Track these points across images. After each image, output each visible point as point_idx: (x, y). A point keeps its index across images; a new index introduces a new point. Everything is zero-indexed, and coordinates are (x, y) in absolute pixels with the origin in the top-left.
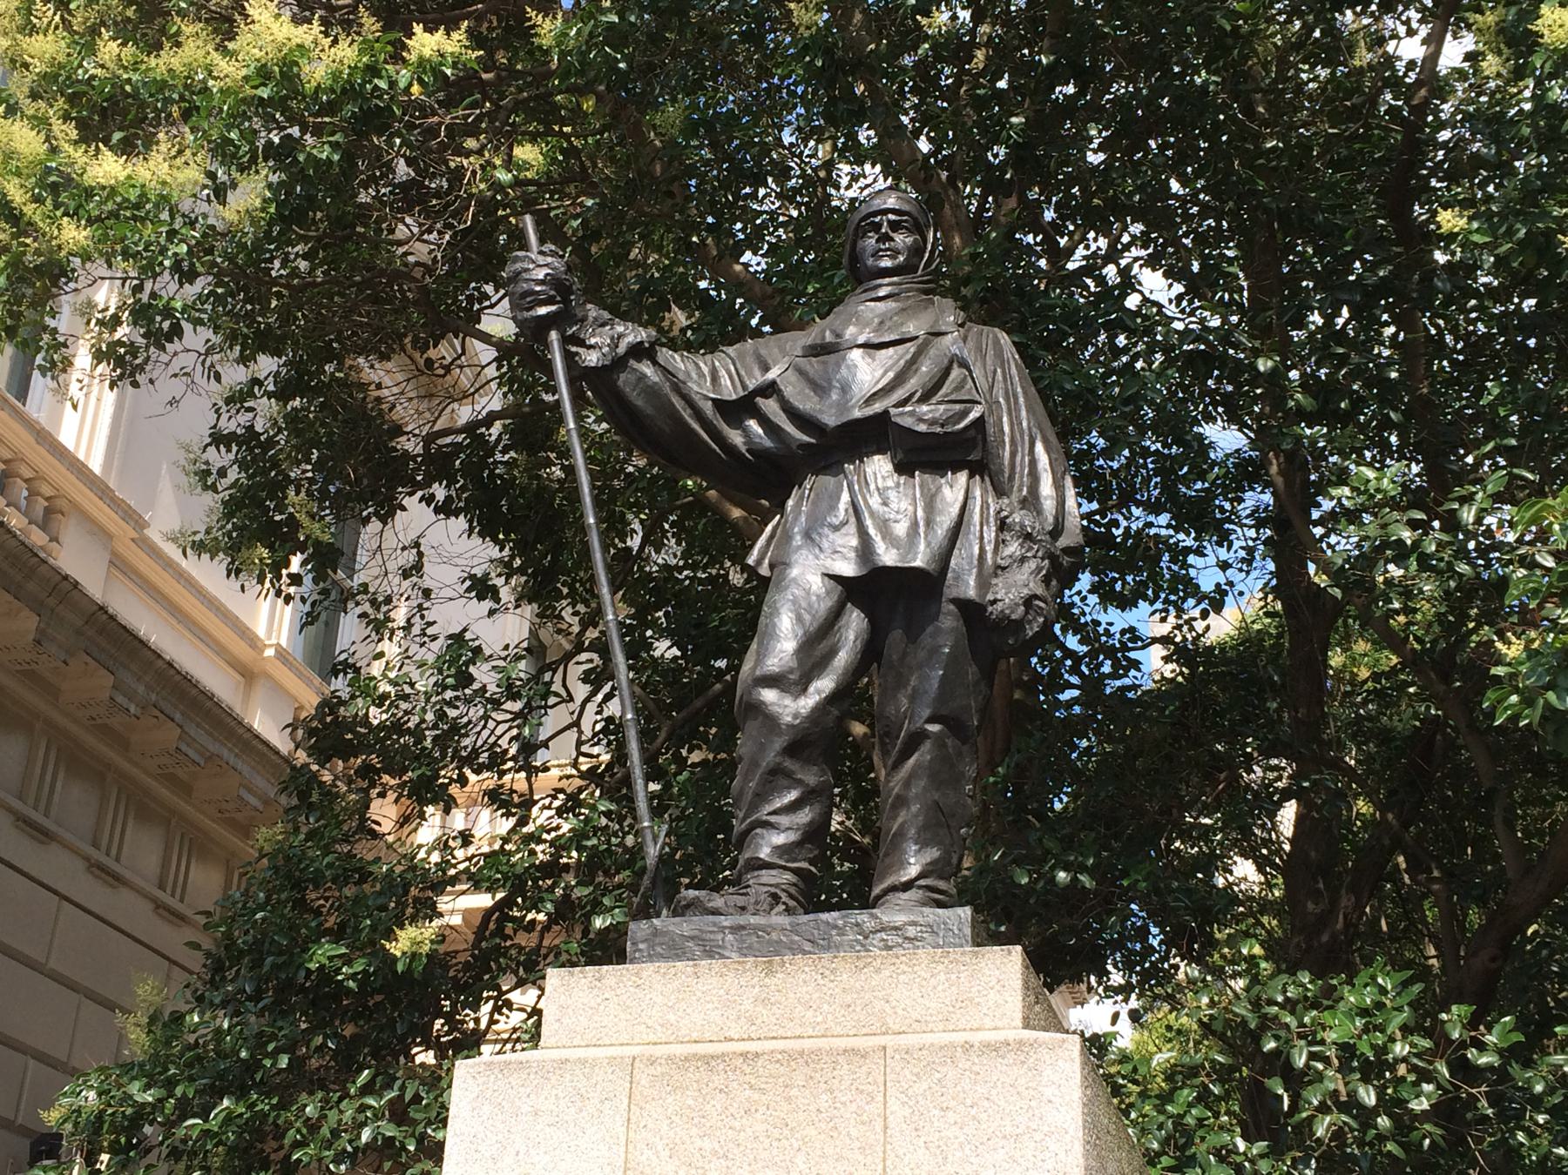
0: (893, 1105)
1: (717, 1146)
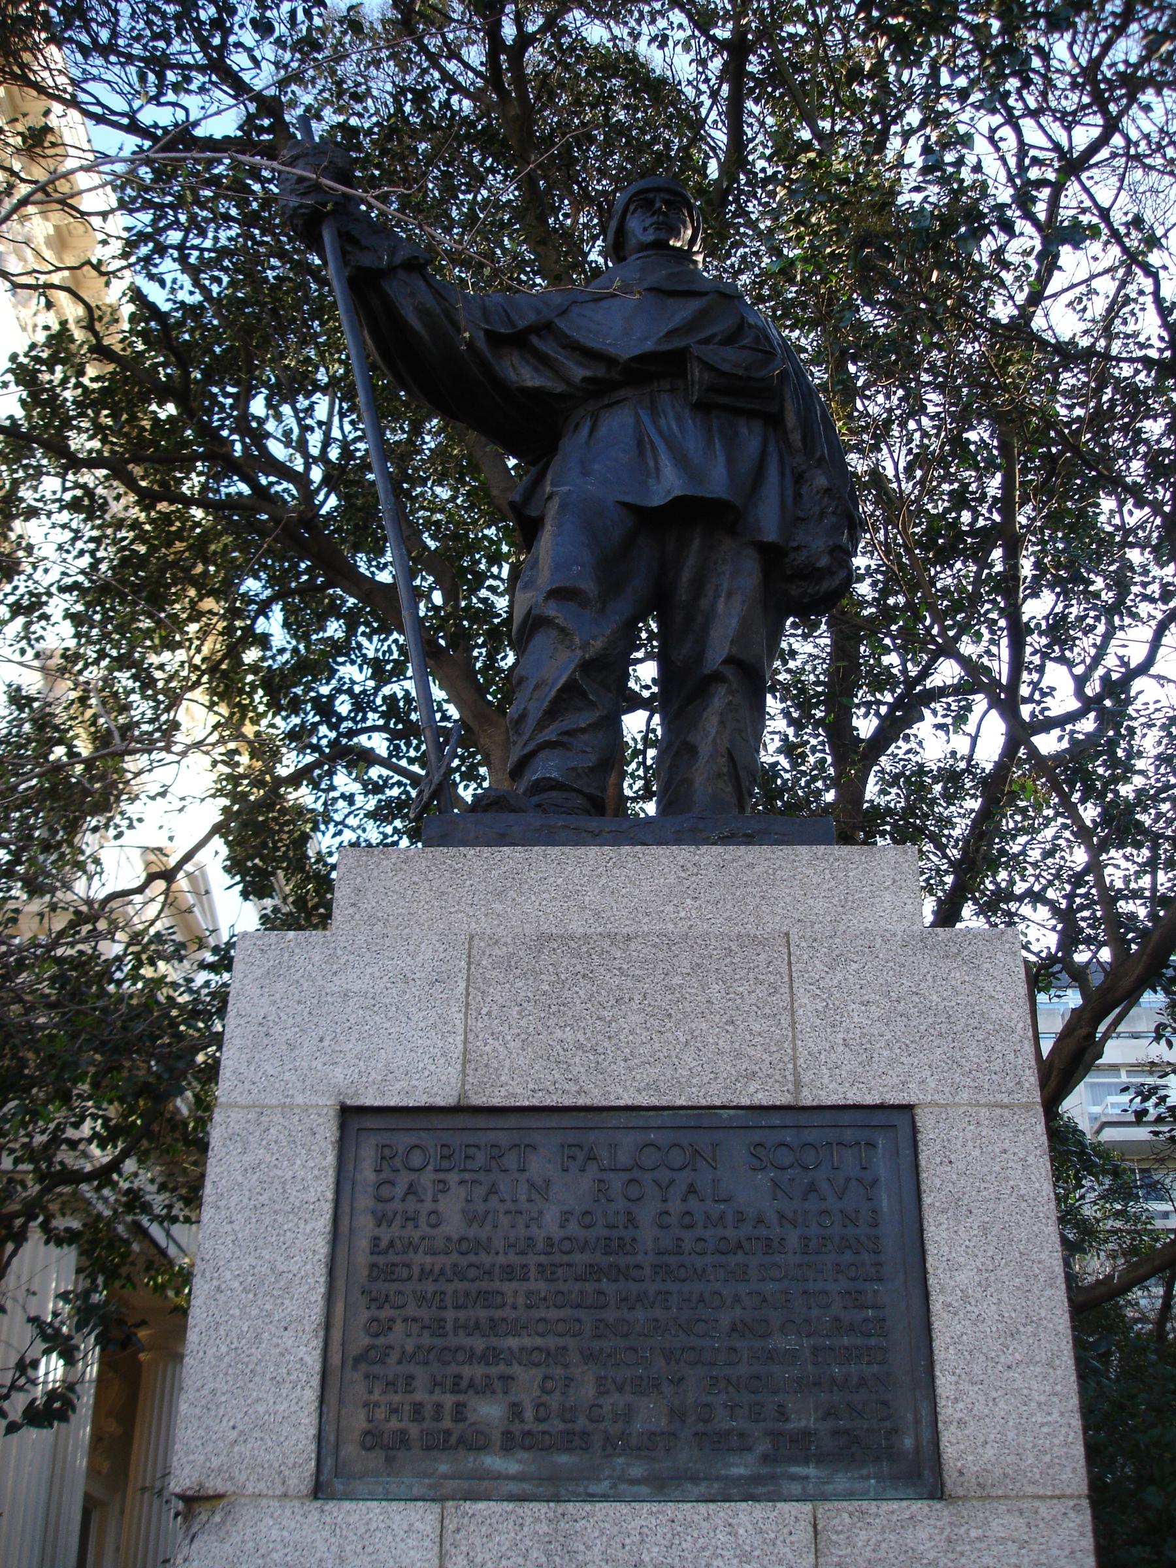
0: (803, 998)
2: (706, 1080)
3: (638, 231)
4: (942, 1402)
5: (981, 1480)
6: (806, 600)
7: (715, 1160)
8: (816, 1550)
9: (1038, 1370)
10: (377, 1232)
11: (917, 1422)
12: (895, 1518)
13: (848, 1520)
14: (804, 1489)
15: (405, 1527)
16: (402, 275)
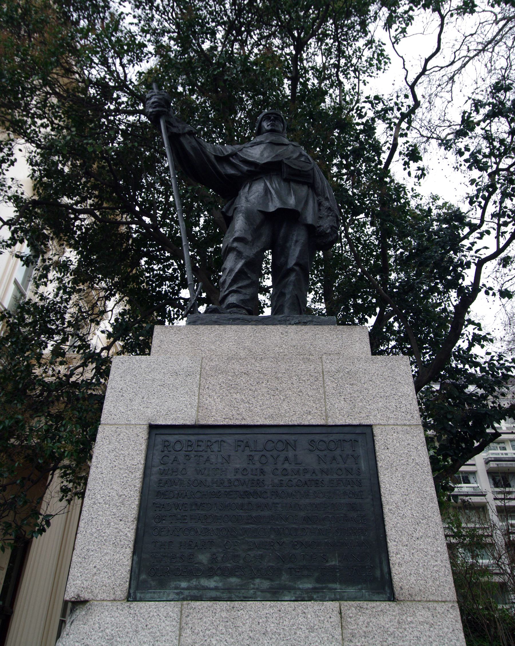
3: (266, 127)
4: (391, 554)
7: (295, 446)
8: (342, 626)
13: (354, 611)
15: (165, 615)
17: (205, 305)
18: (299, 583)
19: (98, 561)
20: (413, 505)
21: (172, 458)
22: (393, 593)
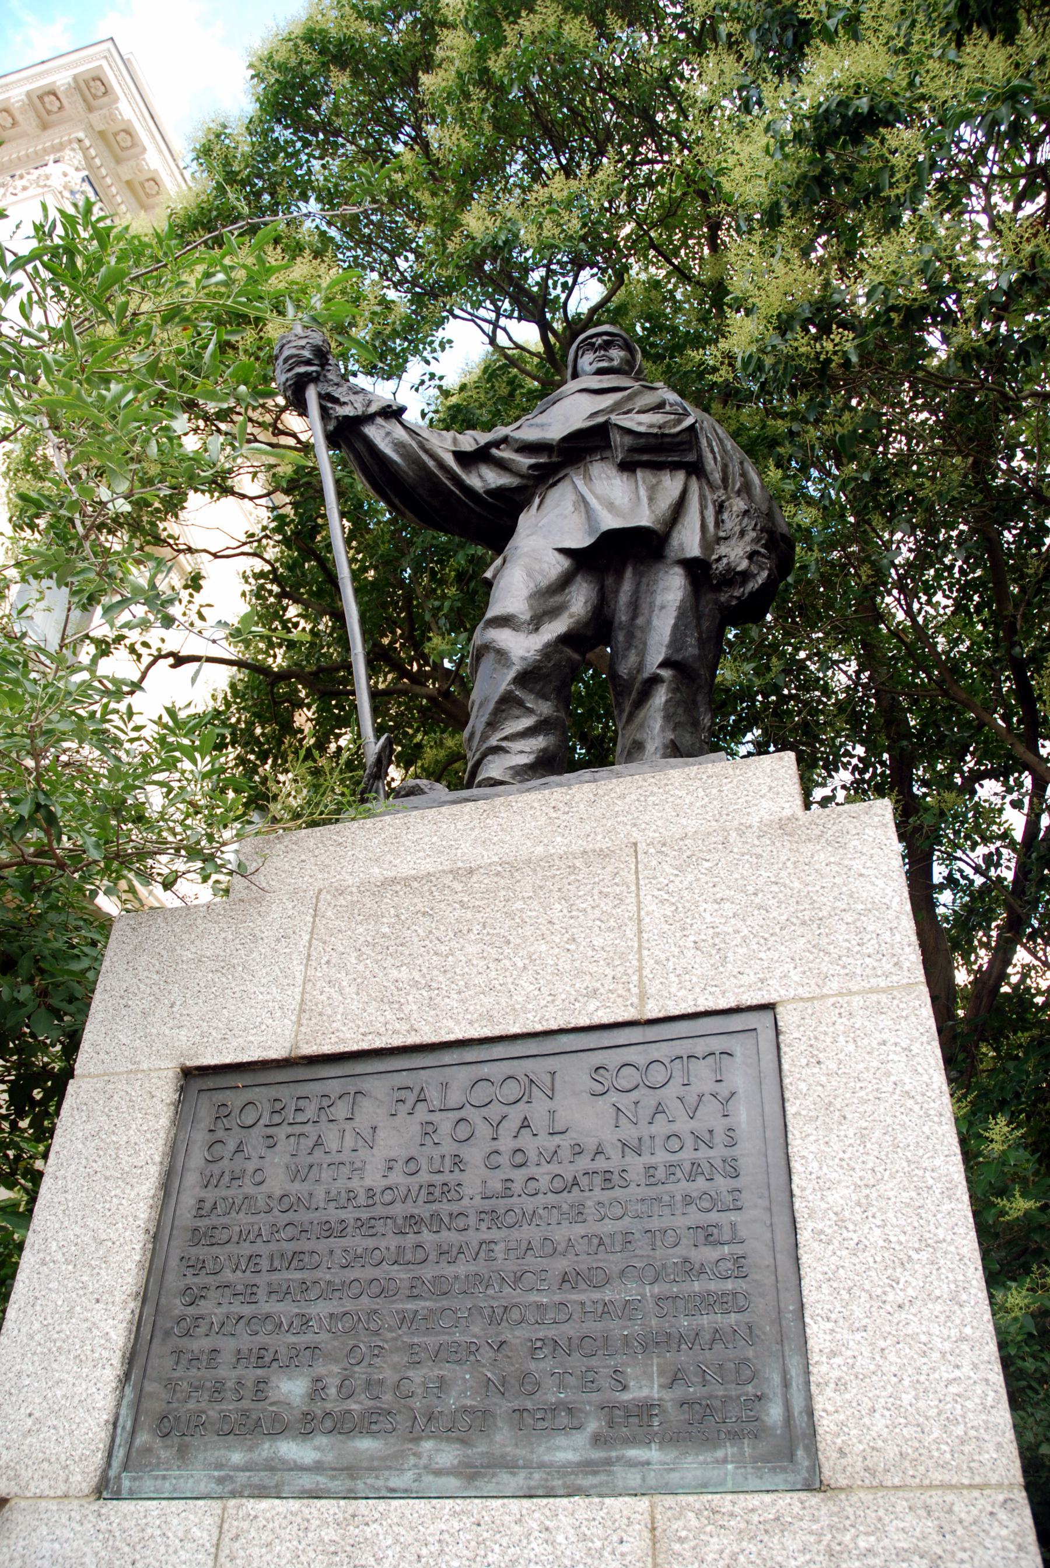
0: (650, 904)
1: (417, 976)
2: (543, 1003)
4: (814, 1358)
5: (869, 1463)
6: (734, 603)
9: (939, 1308)
10: (203, 1194)
11: (786, 1384)
12: (755, 1518)
13: (694, 1522)
14: (643, 1479)
15: (181, 1534)
16: (379, 420)
17: (1019, 947)
18: (542, 1449)
19: (37, 1401)
20: (890, 1214)
21: (232, 1146)
22: (815, 1467)
